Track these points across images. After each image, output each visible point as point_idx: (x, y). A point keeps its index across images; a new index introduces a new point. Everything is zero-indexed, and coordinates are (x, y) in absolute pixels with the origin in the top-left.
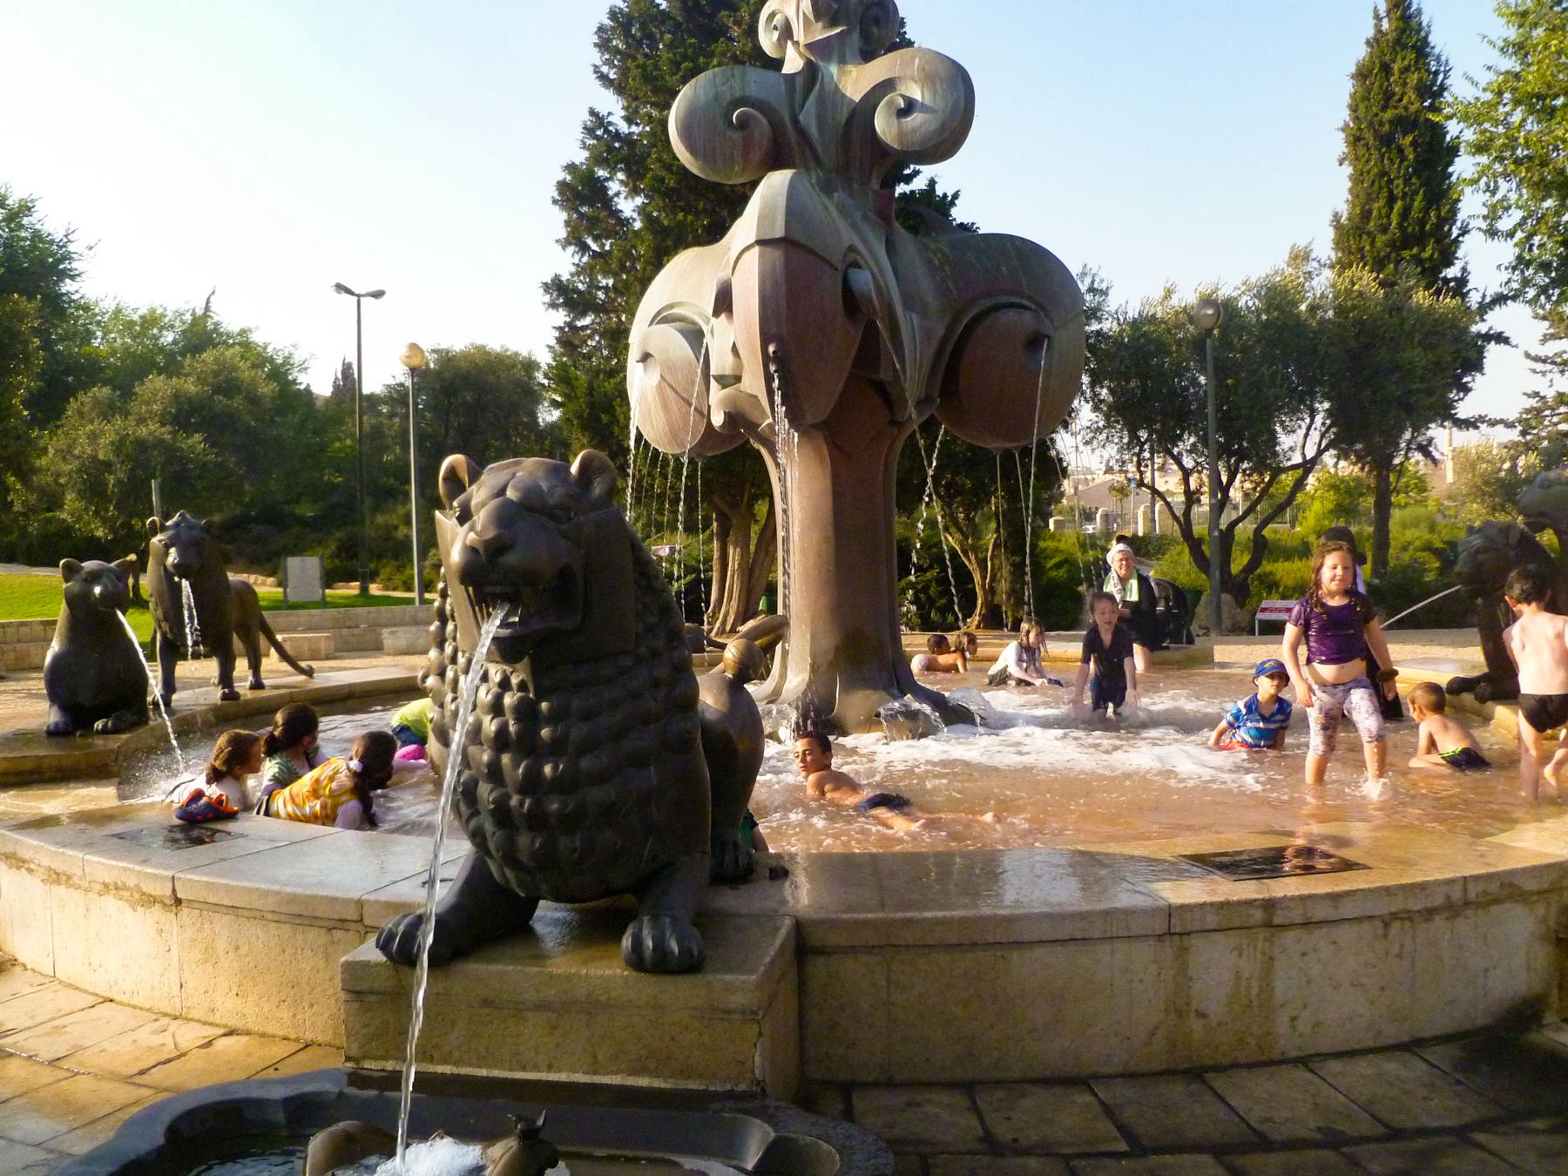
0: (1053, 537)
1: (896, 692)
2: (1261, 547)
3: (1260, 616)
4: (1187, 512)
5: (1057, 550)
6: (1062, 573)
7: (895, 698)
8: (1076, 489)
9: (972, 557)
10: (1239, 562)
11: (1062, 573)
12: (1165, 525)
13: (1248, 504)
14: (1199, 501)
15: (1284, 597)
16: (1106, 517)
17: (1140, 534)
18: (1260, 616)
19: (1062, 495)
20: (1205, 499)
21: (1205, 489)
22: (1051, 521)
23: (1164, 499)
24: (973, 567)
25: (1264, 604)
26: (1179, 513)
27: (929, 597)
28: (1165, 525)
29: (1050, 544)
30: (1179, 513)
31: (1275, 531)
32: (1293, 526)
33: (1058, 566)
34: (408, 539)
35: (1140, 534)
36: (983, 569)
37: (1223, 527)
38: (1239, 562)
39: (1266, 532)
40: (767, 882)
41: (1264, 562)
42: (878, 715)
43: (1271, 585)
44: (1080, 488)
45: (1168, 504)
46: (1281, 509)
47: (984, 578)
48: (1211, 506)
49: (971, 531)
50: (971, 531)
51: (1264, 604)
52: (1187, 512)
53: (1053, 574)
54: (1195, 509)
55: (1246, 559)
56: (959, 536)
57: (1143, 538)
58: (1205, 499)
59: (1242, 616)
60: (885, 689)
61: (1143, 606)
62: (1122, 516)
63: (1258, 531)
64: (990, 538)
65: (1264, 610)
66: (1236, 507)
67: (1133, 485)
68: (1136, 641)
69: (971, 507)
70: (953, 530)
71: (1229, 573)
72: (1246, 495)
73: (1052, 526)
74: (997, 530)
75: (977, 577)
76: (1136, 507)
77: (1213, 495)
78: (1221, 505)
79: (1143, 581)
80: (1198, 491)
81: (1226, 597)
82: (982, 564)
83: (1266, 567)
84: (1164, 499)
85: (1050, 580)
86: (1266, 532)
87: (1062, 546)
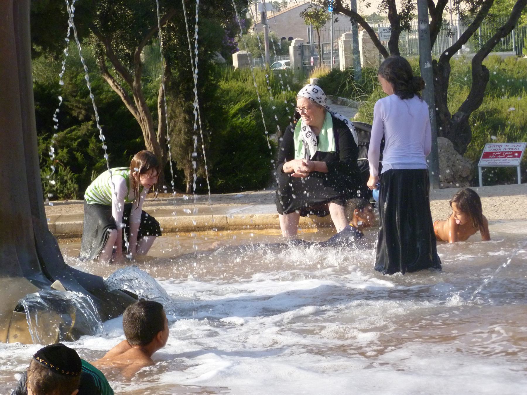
0: (236, 75)
1: (41, 278)
2: (481, 80)
3: (483, 163)
4: (394, 42)
5: (242, 92)
6: (249, 119)
7: (39, 285)
8: (264, 15)
9: (138, 105)
10: (457, 98)
11: (249, 119)
12: (368, 57)
13: (465, 28)
14: (407, 27)
15: (511, 139)
16: (300, 48)
17: (342, 68)
18: (483, 163)
19: (247, 24)
20: (414, 24)
21: (415, 12)
22: (235, 56)
23: (365, 26)
24: (140, 116)
25: (487, 149)
26: (385, 42)
27: (86, 155)
28: (368, 57)
29: (234, 85)
30: (385, 42)
31: (500, 61)
32: (519, 54)
33: (244, 111)
34: (161, 12)
35: (342, 68)
36: (152, 118)
37: (437, 57)
38: (457, 98)
39: (489, 62)
40: (374, 339)
41: (487, 99)
42: (21, 308)
43: (496, 125)
44: (269, 14)
45: (371, 32)
46: (505, 31)
47: (154, 129)
48: (420, 31)
49: (133, 71)
50: (133, 71)
51: (487, 149)
52: (394, 42)
53: (239, 121)
54: (405, 38)
55: (464, 95)
56: (119, 79)
57: (346, 73)
58: (414, 24)
59: (462, 164)
60: (28, 275)
61: (342, 157)
62: (321, 47)
63: (477, 61)
64: (159, 81)
65: (488, 155)
66: (451, 34)
67: (330, 10)
68: (332, 200)
69: (136, 42)
70: (113, 70)
71: (447, 114)
72: (462, 17)
73: (235, 63)
74: (168, 72)
75: (145, 129)
76: (336, 37)
77: (422, 19)
78: (434, 29)
79: (340, 127)
80: (406, 16)
81: (443, 141)
82: (151, 111)
83: (489, 104)
84: (365, 26)
85: (234, 128)
86: (489, 62)
87: (248, 86)
